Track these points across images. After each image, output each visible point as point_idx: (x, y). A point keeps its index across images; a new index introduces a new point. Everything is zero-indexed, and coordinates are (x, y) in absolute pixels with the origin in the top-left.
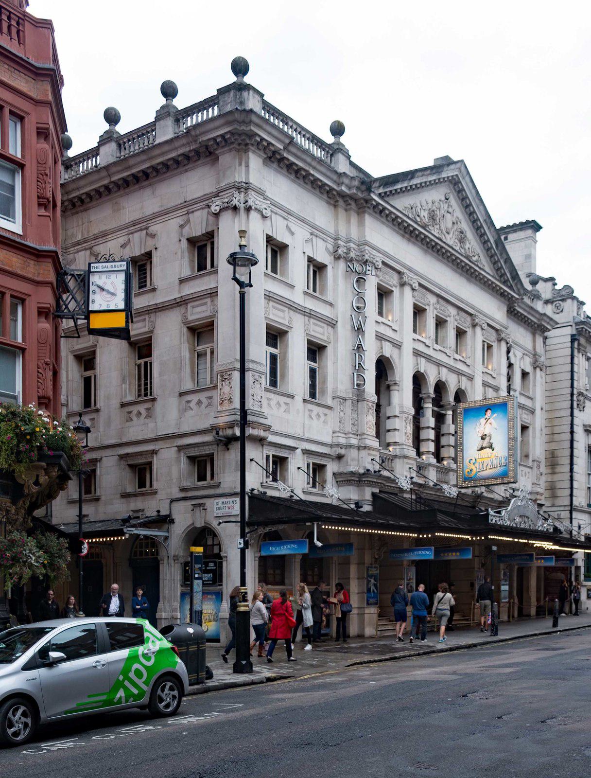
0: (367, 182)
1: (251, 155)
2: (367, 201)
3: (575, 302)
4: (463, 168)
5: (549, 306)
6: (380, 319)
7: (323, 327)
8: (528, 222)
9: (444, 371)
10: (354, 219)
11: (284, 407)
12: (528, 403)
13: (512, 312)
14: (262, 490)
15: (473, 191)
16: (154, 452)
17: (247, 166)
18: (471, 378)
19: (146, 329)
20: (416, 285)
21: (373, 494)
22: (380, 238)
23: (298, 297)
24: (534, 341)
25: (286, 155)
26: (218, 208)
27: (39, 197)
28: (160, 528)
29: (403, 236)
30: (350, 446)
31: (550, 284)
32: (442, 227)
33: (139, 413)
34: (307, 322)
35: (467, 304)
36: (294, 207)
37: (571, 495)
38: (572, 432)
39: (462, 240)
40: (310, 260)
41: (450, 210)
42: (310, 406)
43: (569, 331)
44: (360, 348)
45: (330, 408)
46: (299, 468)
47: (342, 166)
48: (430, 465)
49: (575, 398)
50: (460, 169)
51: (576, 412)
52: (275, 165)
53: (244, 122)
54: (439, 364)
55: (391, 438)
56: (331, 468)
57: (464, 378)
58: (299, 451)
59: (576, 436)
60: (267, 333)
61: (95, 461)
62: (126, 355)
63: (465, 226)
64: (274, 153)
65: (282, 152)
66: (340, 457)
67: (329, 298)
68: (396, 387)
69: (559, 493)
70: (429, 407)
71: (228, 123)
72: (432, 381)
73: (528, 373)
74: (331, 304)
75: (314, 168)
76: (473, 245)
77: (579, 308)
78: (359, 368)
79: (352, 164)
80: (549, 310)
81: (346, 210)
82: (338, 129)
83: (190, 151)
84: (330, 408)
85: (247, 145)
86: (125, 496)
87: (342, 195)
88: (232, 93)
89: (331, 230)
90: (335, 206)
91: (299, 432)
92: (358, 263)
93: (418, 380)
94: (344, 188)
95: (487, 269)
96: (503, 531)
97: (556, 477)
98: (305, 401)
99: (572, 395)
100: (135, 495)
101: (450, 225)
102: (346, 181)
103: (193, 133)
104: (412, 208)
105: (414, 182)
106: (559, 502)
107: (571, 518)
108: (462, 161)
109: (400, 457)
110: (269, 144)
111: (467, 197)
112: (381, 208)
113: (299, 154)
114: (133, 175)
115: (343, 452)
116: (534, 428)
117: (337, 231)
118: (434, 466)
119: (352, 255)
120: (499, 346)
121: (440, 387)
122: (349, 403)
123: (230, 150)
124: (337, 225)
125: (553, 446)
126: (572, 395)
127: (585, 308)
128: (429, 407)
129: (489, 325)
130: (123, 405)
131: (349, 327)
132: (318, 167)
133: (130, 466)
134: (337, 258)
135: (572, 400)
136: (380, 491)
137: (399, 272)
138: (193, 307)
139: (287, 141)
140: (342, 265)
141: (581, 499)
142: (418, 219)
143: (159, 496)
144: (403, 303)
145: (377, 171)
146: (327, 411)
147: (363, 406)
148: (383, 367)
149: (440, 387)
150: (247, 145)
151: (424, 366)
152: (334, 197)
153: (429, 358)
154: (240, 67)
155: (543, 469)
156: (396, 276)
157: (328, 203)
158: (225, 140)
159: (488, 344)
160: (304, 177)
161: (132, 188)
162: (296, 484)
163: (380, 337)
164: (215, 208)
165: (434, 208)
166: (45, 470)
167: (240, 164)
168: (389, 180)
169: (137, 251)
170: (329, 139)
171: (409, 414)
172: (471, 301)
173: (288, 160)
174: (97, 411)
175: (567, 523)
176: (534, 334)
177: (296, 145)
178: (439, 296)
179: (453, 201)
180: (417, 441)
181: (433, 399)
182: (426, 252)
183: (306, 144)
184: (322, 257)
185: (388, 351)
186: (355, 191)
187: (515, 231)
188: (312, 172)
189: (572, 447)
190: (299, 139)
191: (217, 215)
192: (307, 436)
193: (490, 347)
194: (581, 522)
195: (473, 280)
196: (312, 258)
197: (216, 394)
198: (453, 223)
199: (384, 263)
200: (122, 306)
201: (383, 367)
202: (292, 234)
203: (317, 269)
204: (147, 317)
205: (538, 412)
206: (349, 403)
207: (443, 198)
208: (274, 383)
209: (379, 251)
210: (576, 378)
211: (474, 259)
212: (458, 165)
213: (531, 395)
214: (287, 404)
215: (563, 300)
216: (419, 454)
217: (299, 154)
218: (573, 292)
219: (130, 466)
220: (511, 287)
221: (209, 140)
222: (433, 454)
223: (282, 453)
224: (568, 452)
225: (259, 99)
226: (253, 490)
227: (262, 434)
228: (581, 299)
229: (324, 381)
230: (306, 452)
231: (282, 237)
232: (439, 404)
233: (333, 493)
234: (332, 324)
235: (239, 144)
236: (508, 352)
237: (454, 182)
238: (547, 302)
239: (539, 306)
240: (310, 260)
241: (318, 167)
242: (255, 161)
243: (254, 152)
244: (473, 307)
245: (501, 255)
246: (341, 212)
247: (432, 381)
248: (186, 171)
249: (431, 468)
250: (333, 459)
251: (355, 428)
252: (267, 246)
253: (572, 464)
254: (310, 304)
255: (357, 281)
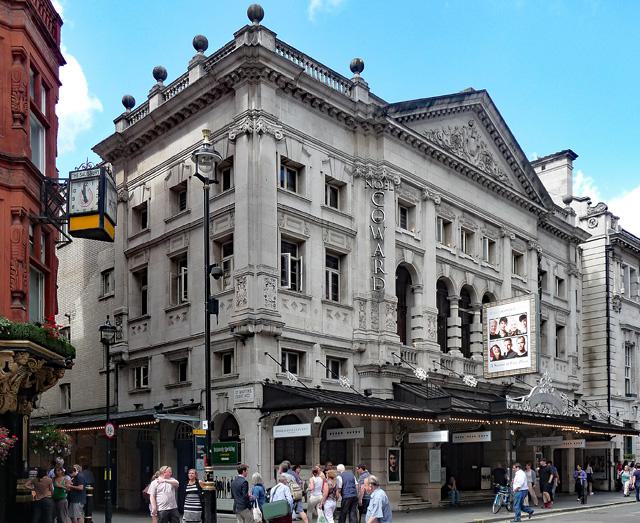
0: (383, 109)
1: (262, 86)
2: (384, 126)
3: (609, 217)
4: (485, 97)
5: (585, 222)
6: (402, 230)
7: (342, 238)
8: (565, 152)
9: (470, 277)
10: (373, 144)
11: (300, 308)
12: (562, 305)
13: (542, 226)
14: (277, 380)
15: (498, 118)
16: (187, 350)
17: (259, 96)
18: (500, 283)
19: (183, 246)
20: (438, 200)
21: (394, 384)
22: (397, 158)
23: (316, 212)
24: (568, 252)
25: (298, 86)
26: (234, 135)
27: (13, 112)
28: (192, 415)
29: (424, 158)
30: (372, 342)
31: (585, 203)
32: (467, 150)
33: (178, 317)
34: (325, 232)
35: (413, 177)
36: (310, 133)
37: (609, 386)
38: (608, 331)
39: (488, 160)
40: (329, 180)
41: (474, 135)
42: (330, 307)
43: (603, 242)
44: (379, 255)
45: (351, 309)
46: (266, 353)
47: (358, 95)
48: (456, 358)
49: (610, 300)
50: (482, 99)
51: (612, 313)
52: (289, 95)
53: (252, 56)
54: (465, 270)
55: (415, 334)
56: (351, 362)
57: (492, 283)
58: (317, 346)
59: (612, 335)
60: (327, 256)
61: (146, 360)
62: (169, 269)
63: (492, 150)
64: (287, 84)
65: (293, 83)
66: (361, 352)
67: (348, 211)
68: (418, 291)
69: (598, 384)
70: (455, 308)
71: (239, 59)
72: (458, 283)
73: (545, 272)
74: (351, 218)
75: (328, 97)
76: (499, 166)
77: (613, 222)
78: (379, 274)
79: (370, 95)
80: (584, 226)
81: (365, 135)
82: (358, 67)
83: (212, 90)
84: (351, 309)
85: (258, 77)
86: (169, 388)
87: (357, 120)
88: (246, 34)
89: (351, 153)
90: (354, 132)
91: (317, 329)
92: (376, 182)
93: (443, 285)
94: (360, 115)
95: (516, 189)
96: (517, 415)
97: (594, 371)
98: (323, 302)
99: (608, 298)
100: (175, 387)
101: (474, 148)
102: (362, 108)
103: (212, 72)
104: (433, 133)
105: (433, 109)
106: (597, 392)
107: (609, 406)
108: (484, 91)
109: (423, 352)
110: (280, 75)
111: (491, 123)
112: (412, 139)
113: (312, 84)
114: (171, 118)
115: (363, 347)
116: (569, 328)
117: (356, 153)
118: (460, 359)
119: (370, 173)
120: (530, 257)
121: (467, 291)
122: (369, 304)
123: (244, 84)
124: (356, 149)
125: (591, 344)
126: (608, 298)
127: (619, 222)
128: (455, 308)
129: (517, 236)
130: (167, 312)
131: (368, 237)
132: (332, 96)
133: (172, 362)
134: (357, 177)
135: (607, 303)
136: (402, 382)
137: (421, 189)
138: (217, 223)
139: (298, 73)
140: (361, 183)
141: (618, 390)
142: (440, 143)
143: (193, 387)
144: (426, 219)
145: (391, 98)
146: (347, 311)
147: (382, 306)
148: (406, 277)
149: (467, 291)
150: (258, 77)
151: (447, 271)
152: (350, 123)
153: (454, 265)
154: (256, 14)
155: (581, 363)
156: (418, 193)
157: (346, 129)
158: (239, 75)
159: (444, 220)
160: (320, 106)
161: (173, 130)
162: (315, 373)
163: (400, 246)
164: (232, 135)
165: (457, 133)
166: (14, 357)
167: (253, 95)
168: (400, 107)
169: (174, 182)
170: (349, 75)
171: (394, 303)
172: (490, 210)
173: (301, 90)
174: (149, 317)
175: (605, 411)
176: (568, 246)
177: (307, 76)
178: (464, 211)
179: (477, 126)
180: (443, 339)
181: (460, 301)
182: (449, 172)
183: (315, 74)
184: (339, 173)
185: (409, 257)
186: (371, 117)
187: (552, 161)
188: (327, 101)
189: (608, 344)
190: (309, 71)
191: (234, 141)
192: (325, 333)
193: (492, 244)
194: (619, 410)
195: (500, 196)
196: (286, 158)
197: (234, 297)
198: (478, 147)
199: (402, 180)
200: (96, 208)
201: (406, 277)
202: (309, 156)
203: (335, 189)
204: (183, 236)
205: (573, 313)
206: (369, 304)
207: (467, 125)
208: (335, 298)
209: (398, 170)
210: (611, 283)
211: (501, 178)
212: (480, 95)
213: (566, 298)
214: (346, 315)
215: (597, 216)
216: (445, 349)
217: (312, 84)
218: (606, 209)
219: (172, 362)
220: (540, 203)
221: (226, 77)
222: (460, 349)
223: (301, 348)
224: (605, 348)
225: (272, 38)
226: (267, 380)
227: (275, 330)
228: (615, 214)
229: (345, 285)
230: (324, 347)
231: (295, 155)
232: (462, 305)
233: (348, 382)
234: (352, 235)
235: (252, 77)
236: (539, 260)
237: (479, 111)
238: (581, 220)
239: (577, 223)
240: (329, 180)
241: (332, 96)
242: (267, 91)
243: (265, 83)
244: (499, 220)
245: (528, 174)
246: (360, 137)
247: (458, 283)
248: (212, 108)
249: (457, 362)
250: (354, 354)
251: (376, 326)
252: (282, 168)
253: (608, 359)
254: (327, 217)
255: (376, 197)
